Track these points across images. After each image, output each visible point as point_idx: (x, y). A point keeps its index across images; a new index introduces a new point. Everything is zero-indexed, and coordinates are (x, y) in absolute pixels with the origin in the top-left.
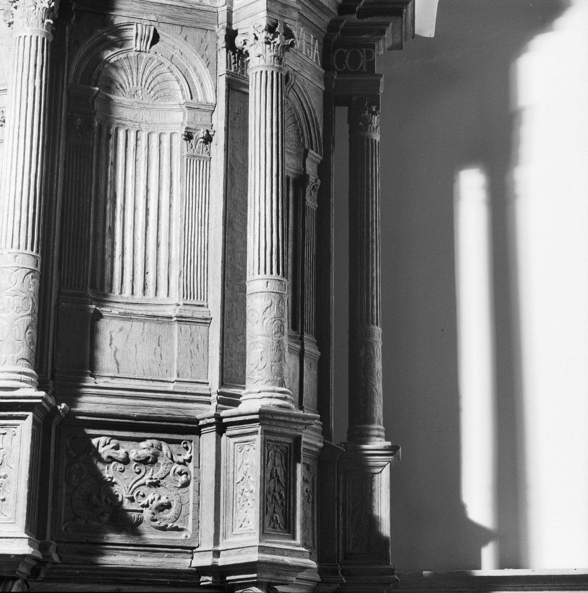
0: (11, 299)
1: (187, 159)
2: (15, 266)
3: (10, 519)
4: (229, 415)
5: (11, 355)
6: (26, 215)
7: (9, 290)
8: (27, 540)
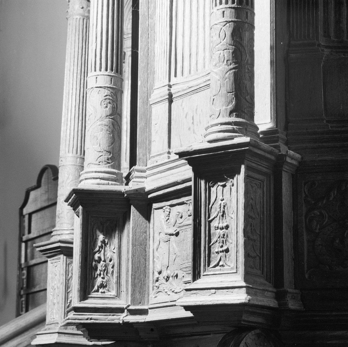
0: (222, 54)
1: (84, 19)
2: (223, 21)
3: (232, 268)
4: (80, 152)
5: (224, 107)
6: (85, 38)
7: (219, 45)
8: (244, 289)
